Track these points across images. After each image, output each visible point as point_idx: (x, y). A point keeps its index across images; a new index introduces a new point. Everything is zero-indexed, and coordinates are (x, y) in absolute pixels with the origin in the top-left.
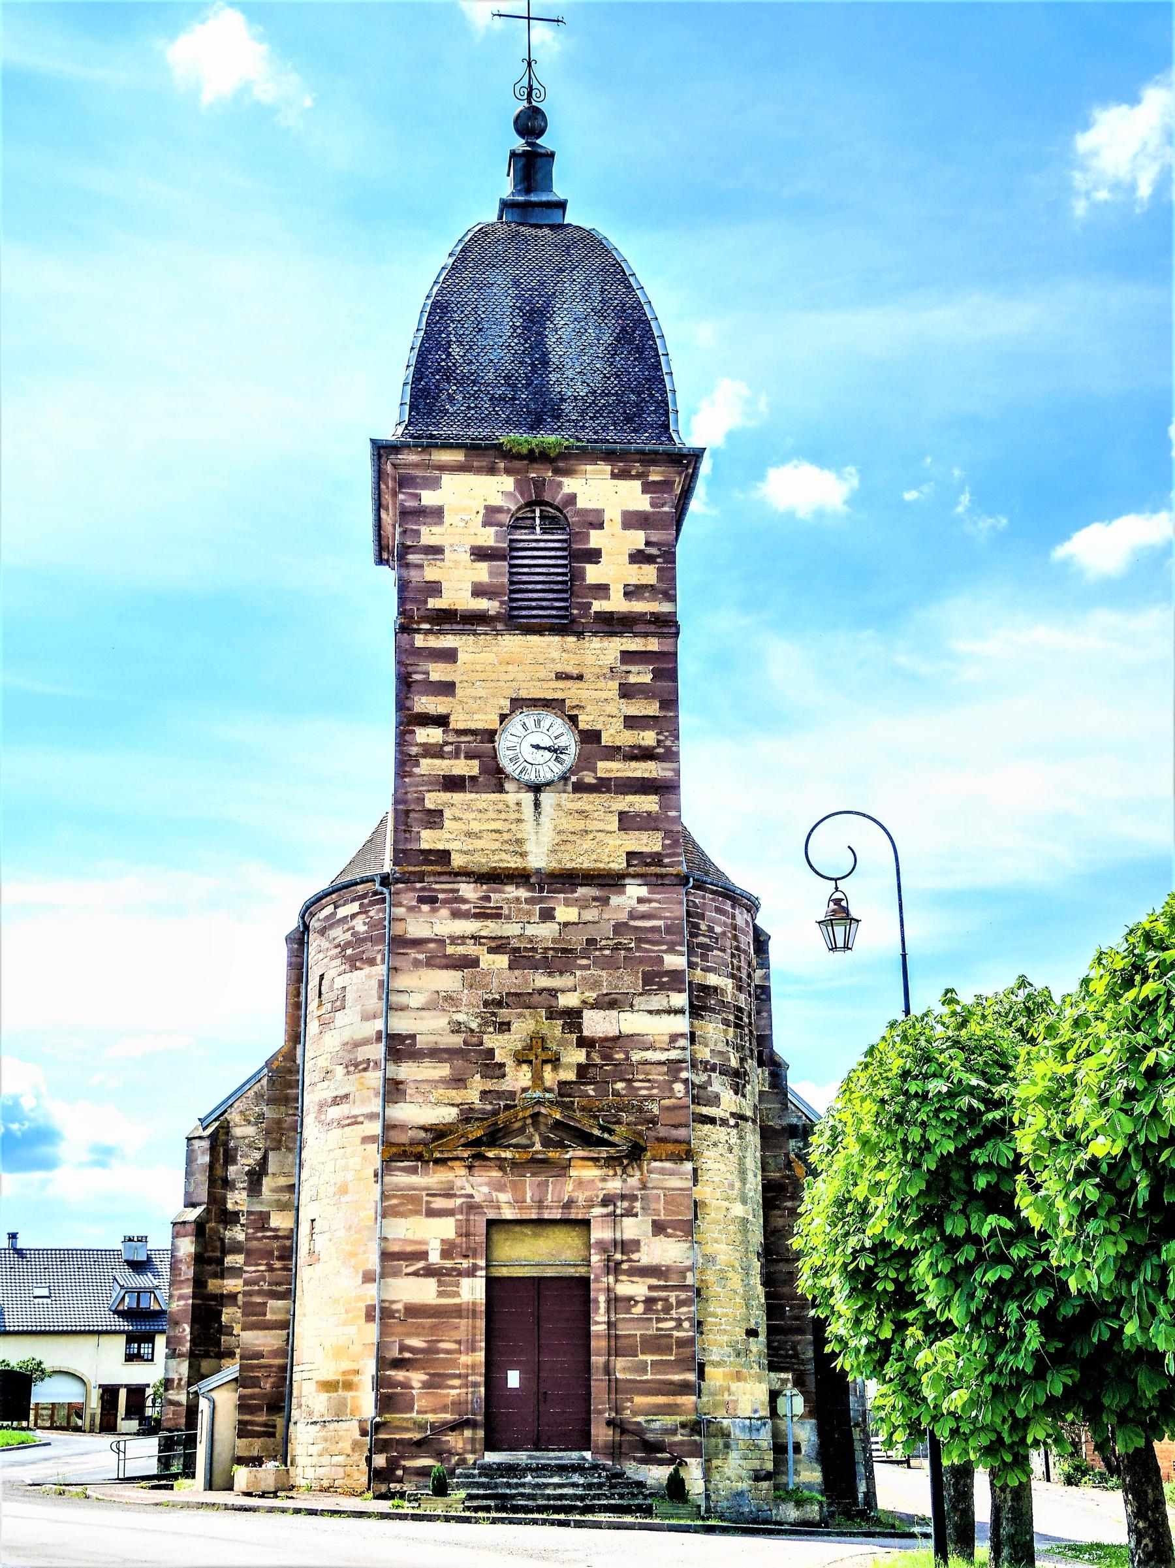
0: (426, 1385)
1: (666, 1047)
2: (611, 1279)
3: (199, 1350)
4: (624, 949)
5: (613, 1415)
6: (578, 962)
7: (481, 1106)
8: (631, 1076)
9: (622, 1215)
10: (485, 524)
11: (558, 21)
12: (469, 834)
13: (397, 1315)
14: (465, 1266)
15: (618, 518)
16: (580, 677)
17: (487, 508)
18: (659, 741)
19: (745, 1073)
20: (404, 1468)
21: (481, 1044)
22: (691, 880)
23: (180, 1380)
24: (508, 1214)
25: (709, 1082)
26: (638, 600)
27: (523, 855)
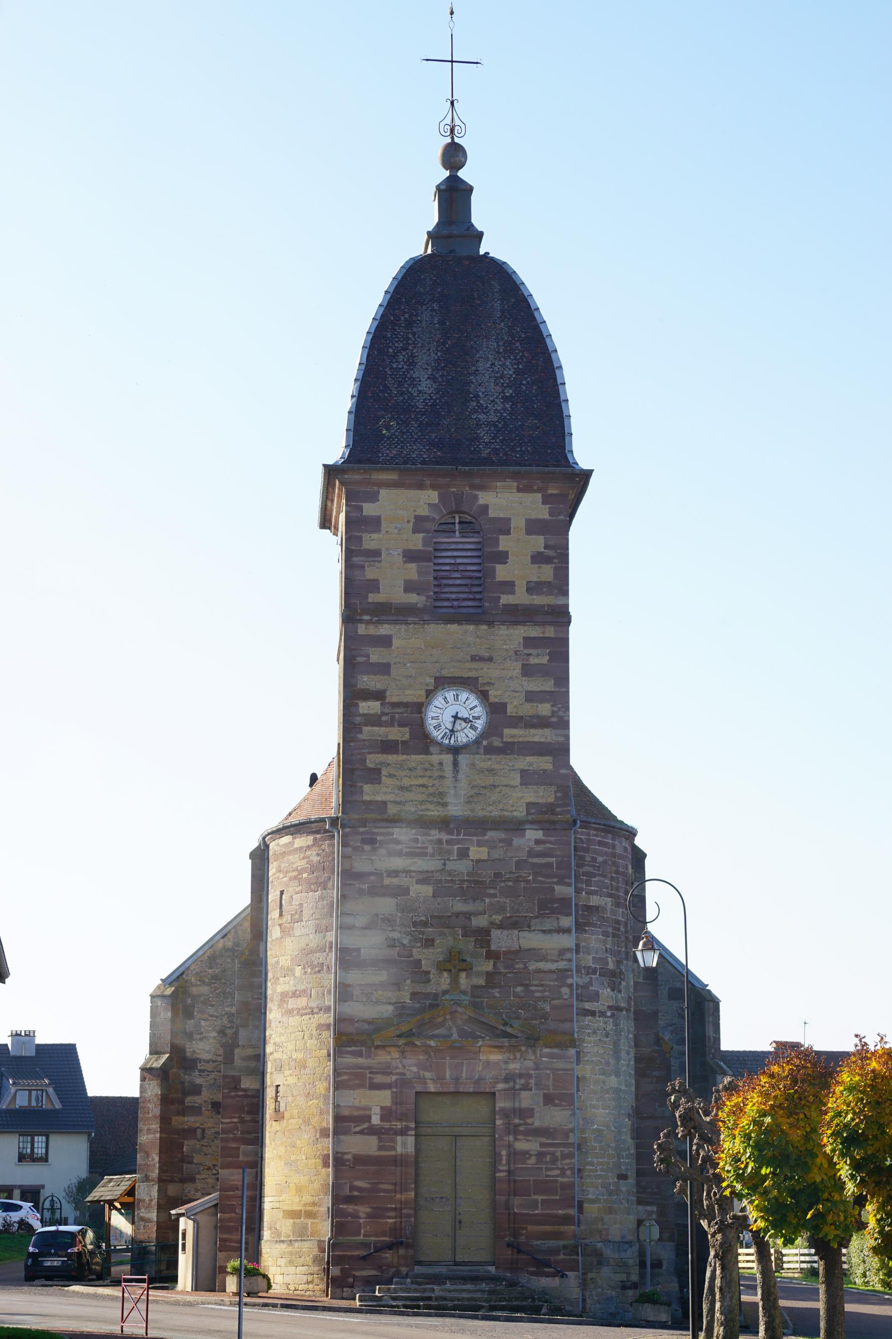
0: (369, 1216)
1: (556, 959)
2: (511, 1138)
3: (166, 1176)
4: (524, 881)
5: (512, 1239)
6: (488, 891)
7: (411, 1005)
8: (528, 982)
9: (521, 1089)
10: (415, 531)
11: (477, 63)
12: (402, 788)
13: (347, 1163)
14: (399, 1127)
15: (522, 524)
16: (490, 659)
17: (416, 517)
18: (553, 712)
19: (621, 973)
20: (354, 1277)
21: (411, 956)
22: (578, 822)
23: (151, 1200)
24: (432, 1088)
25: (590, 983)
26: (537, 594)
27: (445, 805)
